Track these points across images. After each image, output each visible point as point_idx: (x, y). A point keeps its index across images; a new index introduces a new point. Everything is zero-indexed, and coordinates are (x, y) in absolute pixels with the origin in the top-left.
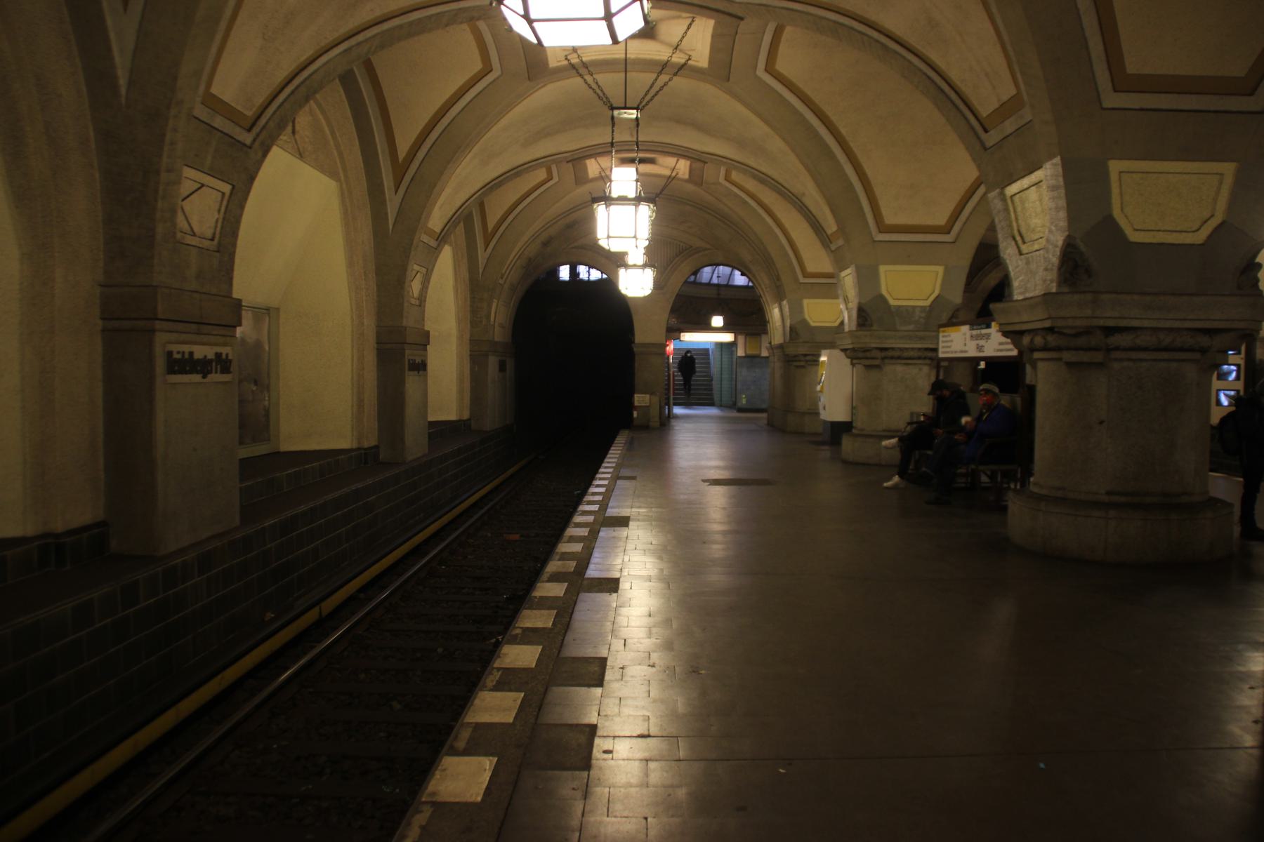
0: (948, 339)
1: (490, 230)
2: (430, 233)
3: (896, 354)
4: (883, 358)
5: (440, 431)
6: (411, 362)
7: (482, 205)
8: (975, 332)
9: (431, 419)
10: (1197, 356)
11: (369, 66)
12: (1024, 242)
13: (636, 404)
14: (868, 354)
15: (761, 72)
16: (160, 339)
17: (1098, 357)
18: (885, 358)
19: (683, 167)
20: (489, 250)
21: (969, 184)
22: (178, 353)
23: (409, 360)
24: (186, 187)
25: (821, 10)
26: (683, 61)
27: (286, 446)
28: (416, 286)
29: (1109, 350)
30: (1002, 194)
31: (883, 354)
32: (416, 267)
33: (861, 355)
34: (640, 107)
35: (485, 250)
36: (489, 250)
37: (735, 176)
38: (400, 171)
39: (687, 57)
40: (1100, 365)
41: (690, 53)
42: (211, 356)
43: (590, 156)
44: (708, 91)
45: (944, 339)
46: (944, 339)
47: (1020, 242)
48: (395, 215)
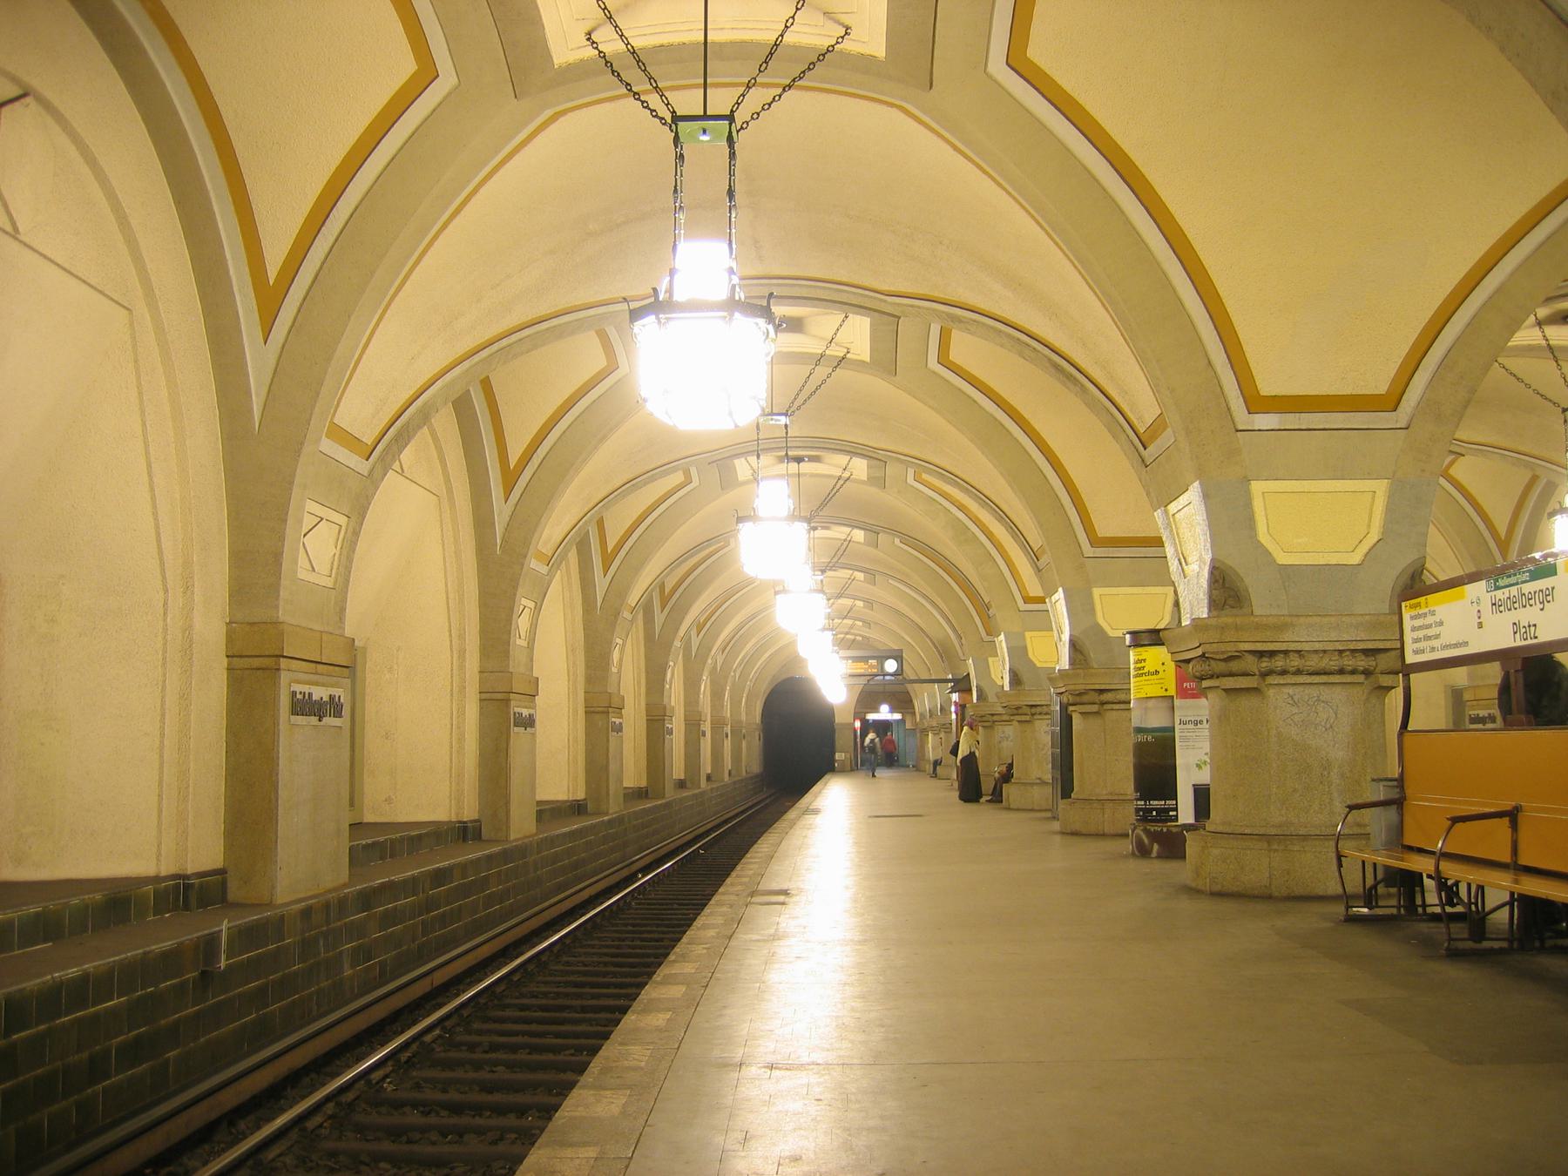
0: (1429, 620)
1: (272, 274)
2: (347, 439)
3: (1295, 662)
4: (1265, 675)
5: (548, 812)
6: (299, 696)
7: (600, 524)
8: (1500, 595)
9: (625, 785)
10: (1361, 678)
11: (486, 385)
12: (1187, 564)
13: (837, 758)
14: (1235, 666)
15: (997, 66)
16: (284, 677)
17: (1095, 708)
18: (1265, 675)
19: (860, 467)
20: (666, 611)
21: (1428, 314)
22: (301, 693)
23: (515, 713)
24: (308, 521)
25: (987, 318)
26: (848, 476)
27: (365, 821)
28: (523, 623)
29: (1033, 715)
30: (1166, 512)
31: (1265, 664)
32: (524, 601)
33: (1220, 667)
34: (740, 117)
35: (698, 636)
36: (666, 611)
37: (965, 348)
38: (270, 302)
39: (846, 350)
40: (1256, 690)
41: (848, 346)
42: (1486, 715)
43: (737, 456)
44: (878, 385)
45: (1418, 623)
46: (1418, 623)
47: (1184, 563)
48: (261, 409)
